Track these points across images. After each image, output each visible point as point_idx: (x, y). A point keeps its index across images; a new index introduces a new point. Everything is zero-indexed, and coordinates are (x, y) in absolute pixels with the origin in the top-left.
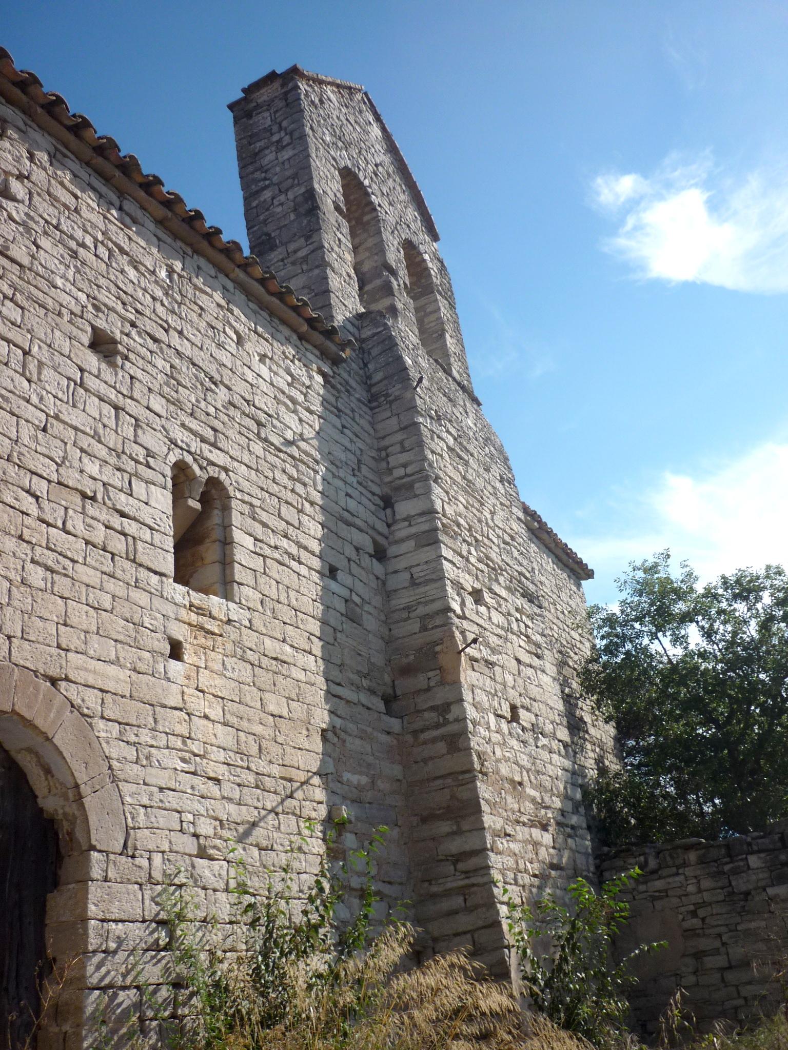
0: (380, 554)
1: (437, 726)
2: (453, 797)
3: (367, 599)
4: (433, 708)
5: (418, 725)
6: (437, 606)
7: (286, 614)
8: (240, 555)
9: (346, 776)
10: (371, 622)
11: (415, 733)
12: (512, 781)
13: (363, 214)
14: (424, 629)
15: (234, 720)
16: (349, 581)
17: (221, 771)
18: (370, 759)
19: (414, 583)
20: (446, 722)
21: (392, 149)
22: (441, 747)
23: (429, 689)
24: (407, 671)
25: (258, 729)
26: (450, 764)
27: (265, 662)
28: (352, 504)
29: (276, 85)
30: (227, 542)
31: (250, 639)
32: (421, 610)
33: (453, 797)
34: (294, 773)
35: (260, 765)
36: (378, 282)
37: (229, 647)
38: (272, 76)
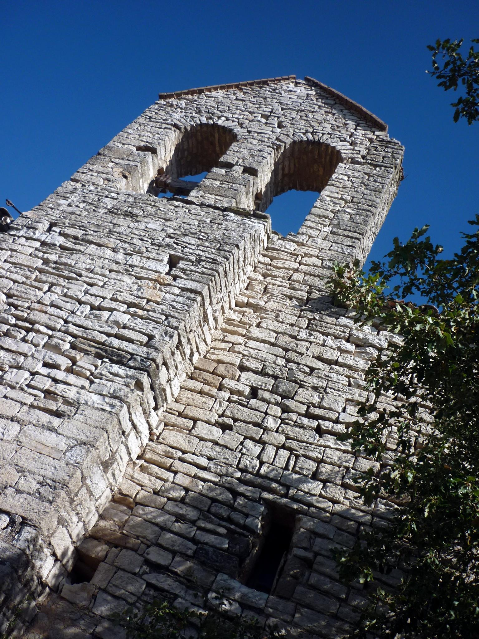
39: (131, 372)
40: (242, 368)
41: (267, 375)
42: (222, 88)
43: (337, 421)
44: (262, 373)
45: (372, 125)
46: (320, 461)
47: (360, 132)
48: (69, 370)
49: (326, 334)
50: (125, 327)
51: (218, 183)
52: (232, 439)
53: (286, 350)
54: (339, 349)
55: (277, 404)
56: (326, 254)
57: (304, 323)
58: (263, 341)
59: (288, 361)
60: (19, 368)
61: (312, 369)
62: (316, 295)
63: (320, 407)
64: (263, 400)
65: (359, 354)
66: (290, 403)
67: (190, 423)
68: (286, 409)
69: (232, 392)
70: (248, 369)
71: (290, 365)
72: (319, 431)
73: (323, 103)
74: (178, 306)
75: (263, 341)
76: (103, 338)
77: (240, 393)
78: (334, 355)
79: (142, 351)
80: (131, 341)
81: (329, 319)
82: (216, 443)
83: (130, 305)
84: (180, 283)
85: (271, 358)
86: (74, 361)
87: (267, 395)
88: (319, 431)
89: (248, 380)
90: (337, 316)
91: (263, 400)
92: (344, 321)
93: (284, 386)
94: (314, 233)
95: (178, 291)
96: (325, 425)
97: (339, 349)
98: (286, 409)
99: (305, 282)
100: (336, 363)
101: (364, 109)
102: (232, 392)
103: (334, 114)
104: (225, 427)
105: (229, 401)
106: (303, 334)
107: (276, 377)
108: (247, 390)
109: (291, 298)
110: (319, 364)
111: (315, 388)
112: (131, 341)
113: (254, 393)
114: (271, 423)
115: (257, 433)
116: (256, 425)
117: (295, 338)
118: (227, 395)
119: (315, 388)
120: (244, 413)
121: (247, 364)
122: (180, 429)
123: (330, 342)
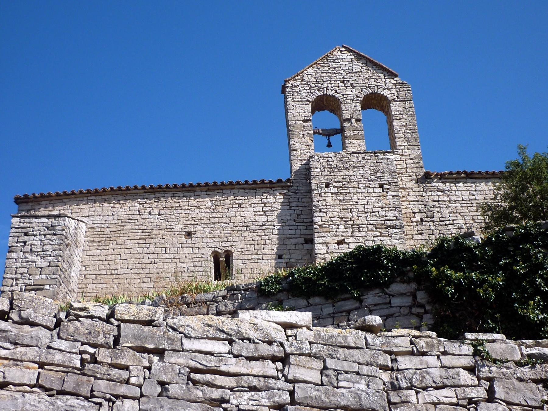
16: (289, 256)
39: (400, 230)
40: (414, 213)
41: (422, 212)
42: (310, 67)
43: (449, 220)
44: (420, 212)
45: (392, 75)
46: (451, 234)
47: (388, 81)
48: (381, 236)
49: (431, 191)
50: (386, 216)
51: (352, 132)
52: (425, 237)
53: (423, 202)
54: (437, 195)
55: (431, 221)
56: (412, 156)
57: (422, 190)
58: (414, 201)
59: (425, 205)
60: (367, 240)
61: (434, 206)
62: (419, 177)
63: (442, 217)
64: (426, 221)
65: (443, 195)
66: (434, 219)
67: (411, 236)
68: (434, 222)
69: (416, 222)
70: (416, 213)
71: (427, 206)
72: (446, 225)
73: (362, 64)
74: (396, 203)
75: (414, 201)
76: (383, 222)
77: (418, 222)
78: (436, 198)
79: (397, 222)
80: (392, 220)
81: (428, 185)
82: (422, 240)
83: (382, 208)
84: (390, 194)
85: (420, 206)
86: (381, 233)
87: (426, 219)
88: (446, 225)
89: (418, 217)
90: (430, 183)
91: (426, 221)
92: (433, 184)
93: (429, 214)
94: (403, 148)
95: (392, 198)
96: (447, 222)
97: (437, 195)
98: (434, 222)
99: (412, 172)
100: (439, 201)
101: (384, 66)
102: (416, 222)
103: (370, 71)
104: (421, 234)
105: (417, 225)
106: (424, 194)
107: (425, 212)
108: (419, 220)
109: (412, 180)
110: (435, 203)
111: (438, 212)
112: (392, 220)
113: (422, 220)
114: (433, 228)
115: (430, 232)
116: (429, 230)
117: (422, 196)
118: (415, 224)
119: (438, 212)
120: (423, 227)
121: (414, 211)
122: (410, 239)
123: (434, 194)
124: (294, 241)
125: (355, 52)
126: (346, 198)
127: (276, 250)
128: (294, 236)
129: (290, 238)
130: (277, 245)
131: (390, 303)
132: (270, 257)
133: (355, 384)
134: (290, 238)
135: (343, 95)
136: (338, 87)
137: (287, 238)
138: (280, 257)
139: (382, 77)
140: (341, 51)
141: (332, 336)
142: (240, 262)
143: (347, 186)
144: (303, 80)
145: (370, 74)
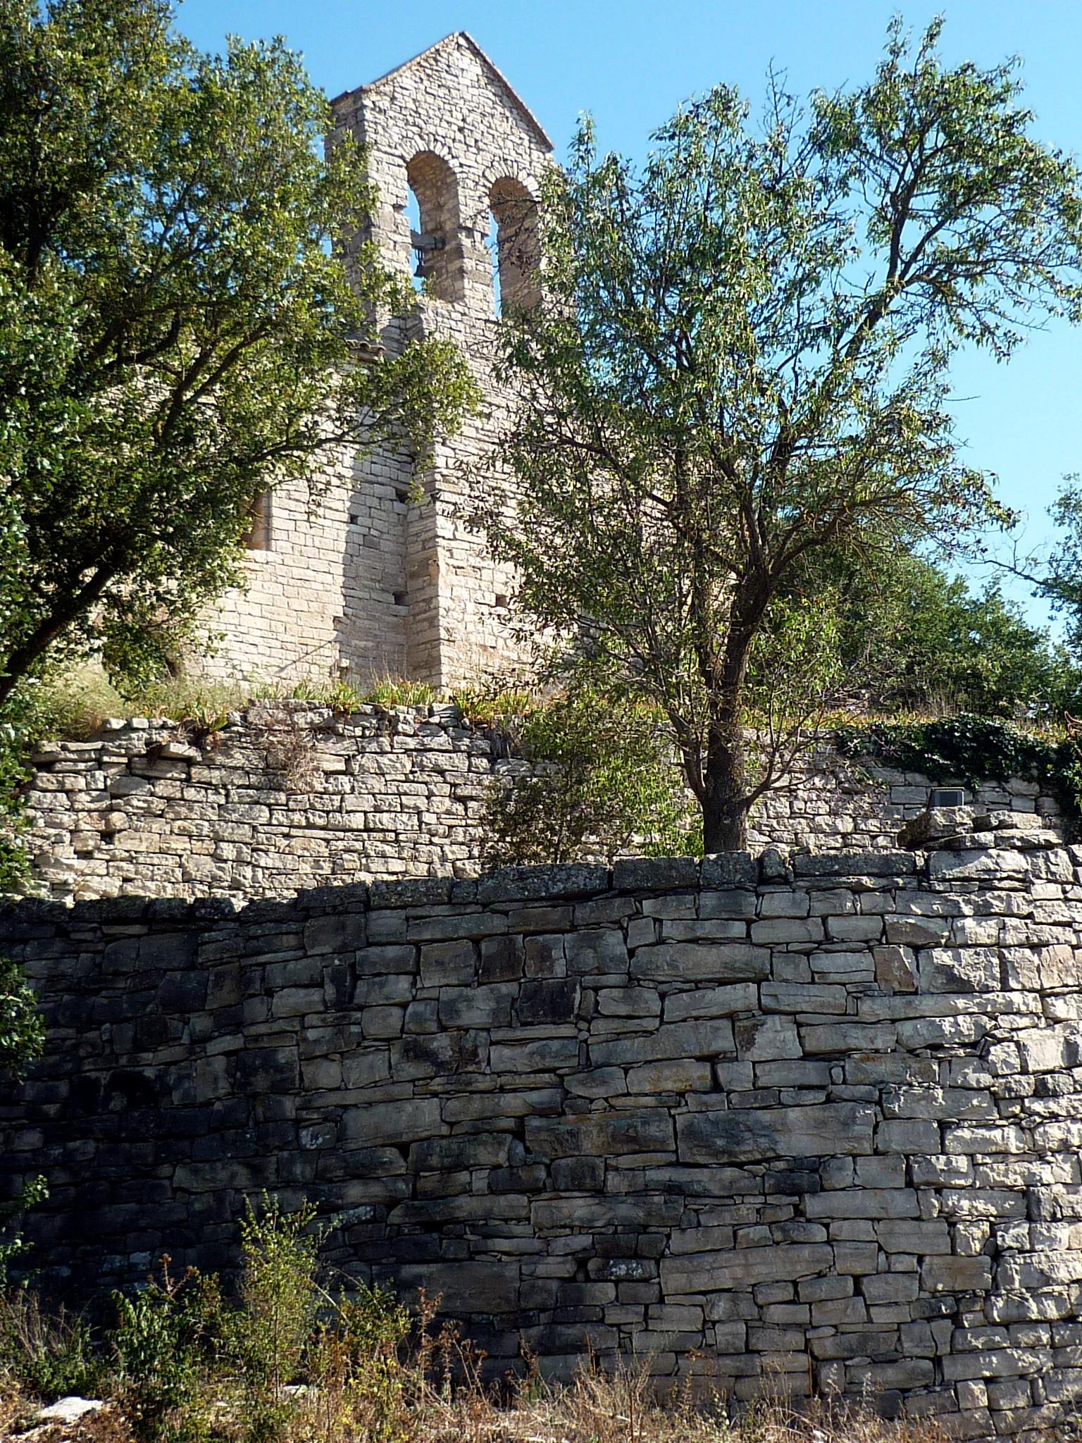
0: (402, 497)
1: (425, 612)
2: (429, 655)
3: (385, 530)
4: (424, 600)
5: (417, 610)
6: (430, 534)
7: (310, 551)
8: (276, 523)
9: (354, 642)
10: (387, 545)
11: (414, 615)
12: (484, 647)
13: (446, 176)
14: (424, 549)
15: (269, 615)
16: (368, 522)
17: (256, 641)
18: (378, 632)
19: (421, 517)
20: (430, 609)
21: (493, 77)
22: (426, 624)
23: (423, 588)
24: (413, 576)
25: (284, 619)
26: (428, 635)
27: (292, 582)
28: (376, 468)
29: (350, 100)
30: (269, 516)
31: (281, 570)
32: (424, 536)
33: (429, 655)
34: (309, 641)
35: (287, 638)
36: (453, 244)
37: (267, 577)
38: (346, 95)
47: (535, 154)
124: (378, 489)
125: (485, 61)
126: (487, 427)
127: (348, 504)
128: (380, 479)
129: (372, 483)
130: (351, 493)
131: (1009, 804)
132: (337, 516)
133: (178, 795)
134: (372, 483)
135: (461, 165)
136: (454, 140)
137: (367, 482)
138: (353, 519)
139: (526, 143)
140: (459, 46)
141: (689, 767)
142: (285, 514)
143: (488, 399)
144: (393, 99)
145: (506, 127)
